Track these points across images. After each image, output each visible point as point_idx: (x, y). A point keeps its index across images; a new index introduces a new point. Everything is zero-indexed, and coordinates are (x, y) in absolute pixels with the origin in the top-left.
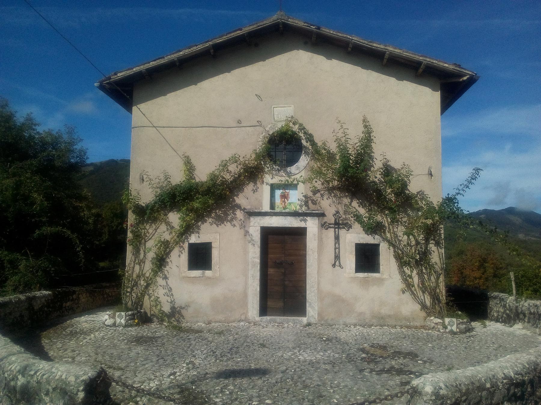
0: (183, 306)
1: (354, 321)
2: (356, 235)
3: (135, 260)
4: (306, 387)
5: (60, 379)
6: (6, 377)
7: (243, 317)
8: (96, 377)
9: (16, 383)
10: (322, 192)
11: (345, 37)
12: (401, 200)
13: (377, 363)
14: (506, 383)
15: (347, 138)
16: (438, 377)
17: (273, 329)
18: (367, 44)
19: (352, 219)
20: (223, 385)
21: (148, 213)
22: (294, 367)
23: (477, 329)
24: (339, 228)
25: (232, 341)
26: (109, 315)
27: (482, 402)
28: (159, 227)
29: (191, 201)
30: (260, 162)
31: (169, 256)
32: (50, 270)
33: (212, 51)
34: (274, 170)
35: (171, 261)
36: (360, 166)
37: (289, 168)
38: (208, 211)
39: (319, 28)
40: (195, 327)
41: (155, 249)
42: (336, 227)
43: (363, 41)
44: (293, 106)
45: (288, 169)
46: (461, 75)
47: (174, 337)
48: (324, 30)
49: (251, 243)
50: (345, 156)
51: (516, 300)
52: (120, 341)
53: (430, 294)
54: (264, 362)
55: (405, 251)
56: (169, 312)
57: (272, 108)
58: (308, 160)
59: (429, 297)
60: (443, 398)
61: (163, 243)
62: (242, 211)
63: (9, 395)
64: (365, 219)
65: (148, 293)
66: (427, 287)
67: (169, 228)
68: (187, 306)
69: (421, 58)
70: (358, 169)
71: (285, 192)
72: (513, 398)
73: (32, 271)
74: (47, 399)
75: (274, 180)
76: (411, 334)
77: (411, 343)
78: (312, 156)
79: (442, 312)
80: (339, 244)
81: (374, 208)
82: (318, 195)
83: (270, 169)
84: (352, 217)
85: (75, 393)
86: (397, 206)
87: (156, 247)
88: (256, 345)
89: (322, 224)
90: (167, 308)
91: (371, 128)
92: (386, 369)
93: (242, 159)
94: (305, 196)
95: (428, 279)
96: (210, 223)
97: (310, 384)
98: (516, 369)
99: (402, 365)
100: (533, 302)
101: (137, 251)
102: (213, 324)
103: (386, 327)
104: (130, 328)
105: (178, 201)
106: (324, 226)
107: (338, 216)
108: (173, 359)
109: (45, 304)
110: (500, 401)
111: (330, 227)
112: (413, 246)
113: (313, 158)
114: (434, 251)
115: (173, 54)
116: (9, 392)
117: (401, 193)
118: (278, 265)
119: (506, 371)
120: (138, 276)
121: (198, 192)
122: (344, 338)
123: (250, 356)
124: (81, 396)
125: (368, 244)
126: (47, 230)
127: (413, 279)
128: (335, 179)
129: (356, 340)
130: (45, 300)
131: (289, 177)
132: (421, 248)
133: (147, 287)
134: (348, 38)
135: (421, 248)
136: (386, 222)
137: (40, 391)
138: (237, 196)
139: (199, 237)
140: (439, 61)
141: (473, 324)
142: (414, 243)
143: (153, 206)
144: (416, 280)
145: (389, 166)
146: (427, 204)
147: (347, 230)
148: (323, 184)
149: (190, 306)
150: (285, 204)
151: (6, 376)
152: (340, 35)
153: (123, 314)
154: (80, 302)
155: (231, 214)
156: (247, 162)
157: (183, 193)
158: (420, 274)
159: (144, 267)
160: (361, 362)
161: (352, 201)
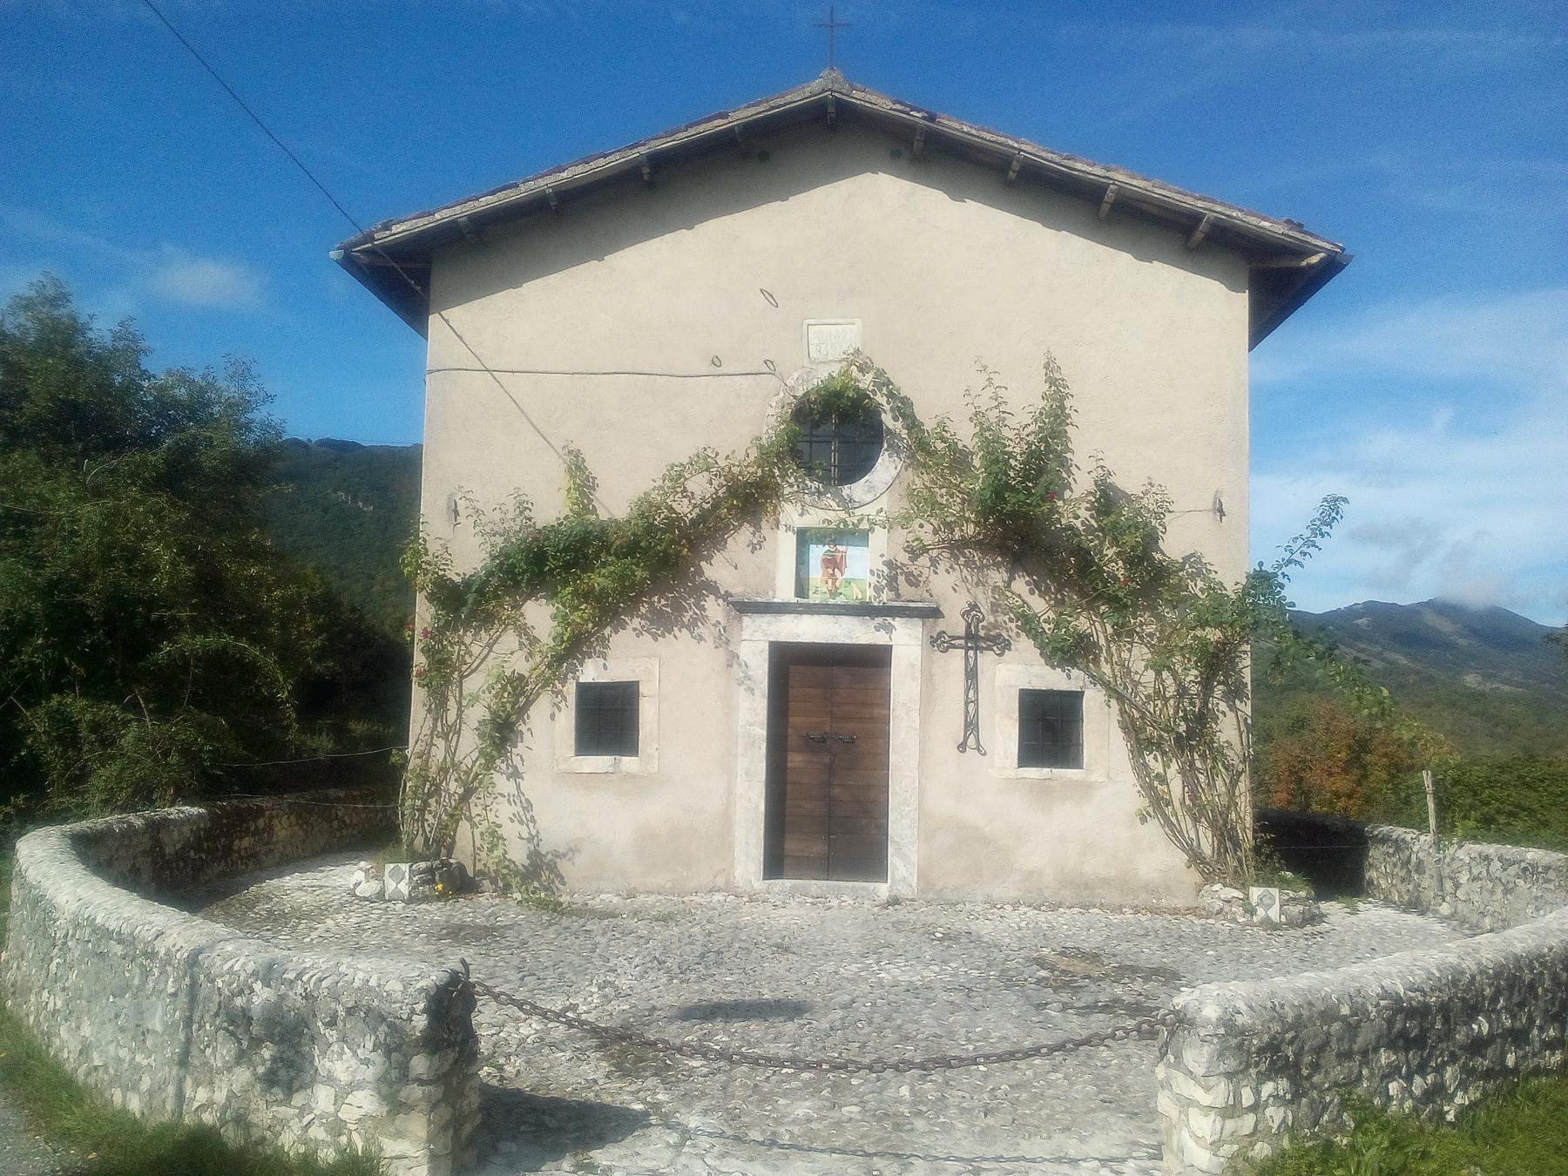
0: (562, 850)
1: (1014, 894)
2: (1021, 667)
3: (435, 726)
4: (906, 1038)
5: (366, 987)
6: (219, 988)
7: (720, 881)
8: (448, 984)
9: (249, 1001)
10: (934, 553)
11: (1001, 144)
12: (1142, 577)
13: (1076, 990)
14: (1385, 1008)
15: (1004, 412)
16: (1231, 988)
17: (802, 912)
18: (1056, 163)
19: (1013, 625)
20: (701, 1033)
21: (470, 601)
22: (871, 997)
23: (1332, 919)
24: (977, 648)
25: (701, 938)
26: (366, 871)
27: (1331, 1047)
28: (498, 639)
29: (584, 571)
30: (770, 470)
31: (525, 717)
32: (201, 751)
33: (646, 170)
34: (806, 491)
35: (529, 729)
36: (1036, 485)
37: (846, 487)
38: (631, 599)
39: (932, 118)
40: (596, 903)
41: (488, 698)
42: (970, 645)
43: (1049, 156)
44: (859, 322)
45: (846, 490)
46: (1304, 251)
47: (547, 928)
48: (946, 122)
49: (744, 686)
50: (996, 457)
51: (1437, 844)
52: (406, 935)
53: (1213, 824)
54: (794, 984)
55: (1149, 712)
56: (523, 866)
57: (805, 326)
58: (899, 468)
59: (1209, 834)
60: (1242, 1033)
61: (510, 681)
62: (720, 601)
63: (230, 1028)
64: (1046, 626)
65: (468, 814)
66: (1204, 806)
67: (527, 643)
68: (573, 850)
69: (1200, 204)
70: (1030, 494)
71: (835, 552)
72: (1401, 1043)
73: (151, 753)
74: (332, 1035)
75: (807, 517)
76: (1163, 927)
77: (1164, 947)
78: (908, 458)
79: (1243, 872)
80: (976, 692)
81: (1069, 596)
82: (924, 560)
83: (795, 488)
84: (1011, 620)
85: (405, 1017)
86: (1133, 592)
87: (490, 693)
88: (764, 946)
89: (932, 637)
90: (518, 855)
91: (1065, 387)
92: (1100, 1004)
93: (722, 463)
94: (890, 564)
95: (1209, 784)
96: (635, 629)
97: (914, 1033)
98: (1411, 979)
99: (1140, 994)
100: (1478, 847)
101: (439, 703)
102: (641, 898)
103: (1097, 911)
104: (424, 906)
105: (551, 570)
106: (940, 642)
107: (975, 615)
108: (561, 976)
109: (192, 839)
110: (1370, 1047)
111: (954, 647)
112: (1171, 697)
113: (912, 463)
114: (1223, 713)
115: (540, 177)
116: (232, 1022)
117: (1141, 559)
118: (816, 744)
119: (1386, 983)
120: (443, 770)
121: (606, 547)
122: (989, 934)
123: (754, 971)
124: (421, 1023)
125: (1052, 690)
126: (193, 643)
127: (1168, 785)
128: (968, 520)
129: (1020, 939)
130: (191, 830)
131: (846, 510)
132: (1192, 704)
133: (465, 798)
134: (1008, 146)
135: (1192, 704)
136: (1101, 635)
137: (315, 1016)
138: (709, 559)
139: (605, 667)
140: (1249, 214)
141: (1325, 906)
142: (1171, 690)
143: (485, 583)
144: (1176, 786)
145: (1112, 487)
146: (1210, 587)
147: (997, 654)
148: (936, 532)
149: (580, 852)
150: (834, 583)
151: (220, 985)
152: (988, 136)
153: (405, 867)
154: (274, 839)
155: (691, 608)
156: (735, 470)
157: (566, 550)
158: (1188, 772)
159: (457, 745)
160: (1038, 987)
161: (1012, 578)
